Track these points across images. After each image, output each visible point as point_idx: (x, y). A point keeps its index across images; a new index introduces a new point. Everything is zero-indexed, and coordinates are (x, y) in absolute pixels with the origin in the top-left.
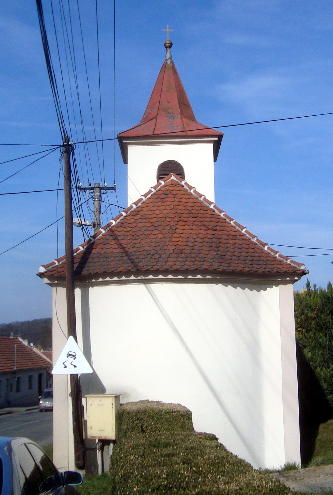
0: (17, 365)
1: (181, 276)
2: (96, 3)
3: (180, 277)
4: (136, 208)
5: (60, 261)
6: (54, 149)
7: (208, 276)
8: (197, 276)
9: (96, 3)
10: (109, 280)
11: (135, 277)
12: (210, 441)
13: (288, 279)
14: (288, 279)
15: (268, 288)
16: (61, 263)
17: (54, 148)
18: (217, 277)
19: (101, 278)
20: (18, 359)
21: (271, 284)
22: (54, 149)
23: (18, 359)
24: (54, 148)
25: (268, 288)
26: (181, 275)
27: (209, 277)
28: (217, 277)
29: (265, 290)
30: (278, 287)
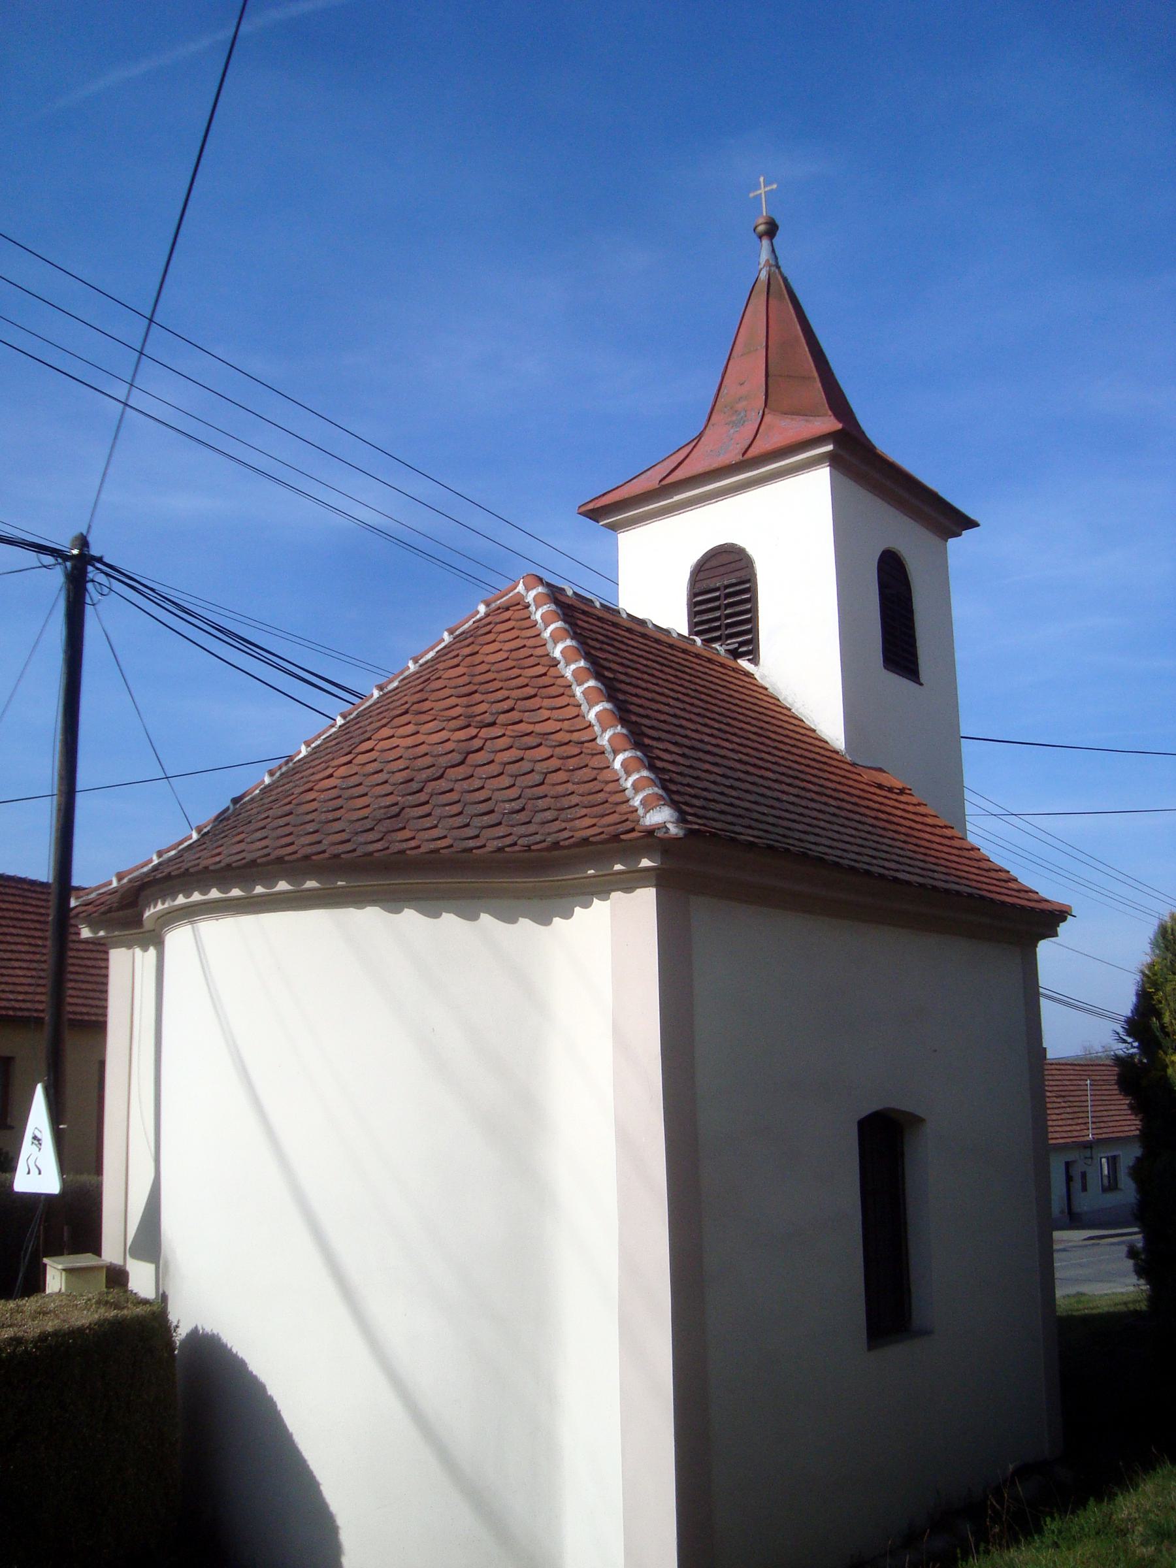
0: (1094, 1117)
1: (314, 882)
2: (129, 346)
3: (214, 894)
4: (381, 696)
5: (126, 877)
6: (693, 444)
7: (308, 882)
8: (230, 891)
9: (129, 346)
10: (218, 896)
11: (221, 892)
12: (1072, 1551)
13: (618, 867)
14: (618, 867)
15: (577, 910)
16: (125, 880)
17: (693, 440)
18: (339, 883)
19: (181, 896)
20: (1083, 1098)
21: (583, 894)
22: (696, 441)
23: (1083, 1098)
24: (693, 440)
25: (577, 910)
26: (239, 888)
27: (311, 884)
28: (339, 883)
29: (567, 914)
30: (609, 901)
